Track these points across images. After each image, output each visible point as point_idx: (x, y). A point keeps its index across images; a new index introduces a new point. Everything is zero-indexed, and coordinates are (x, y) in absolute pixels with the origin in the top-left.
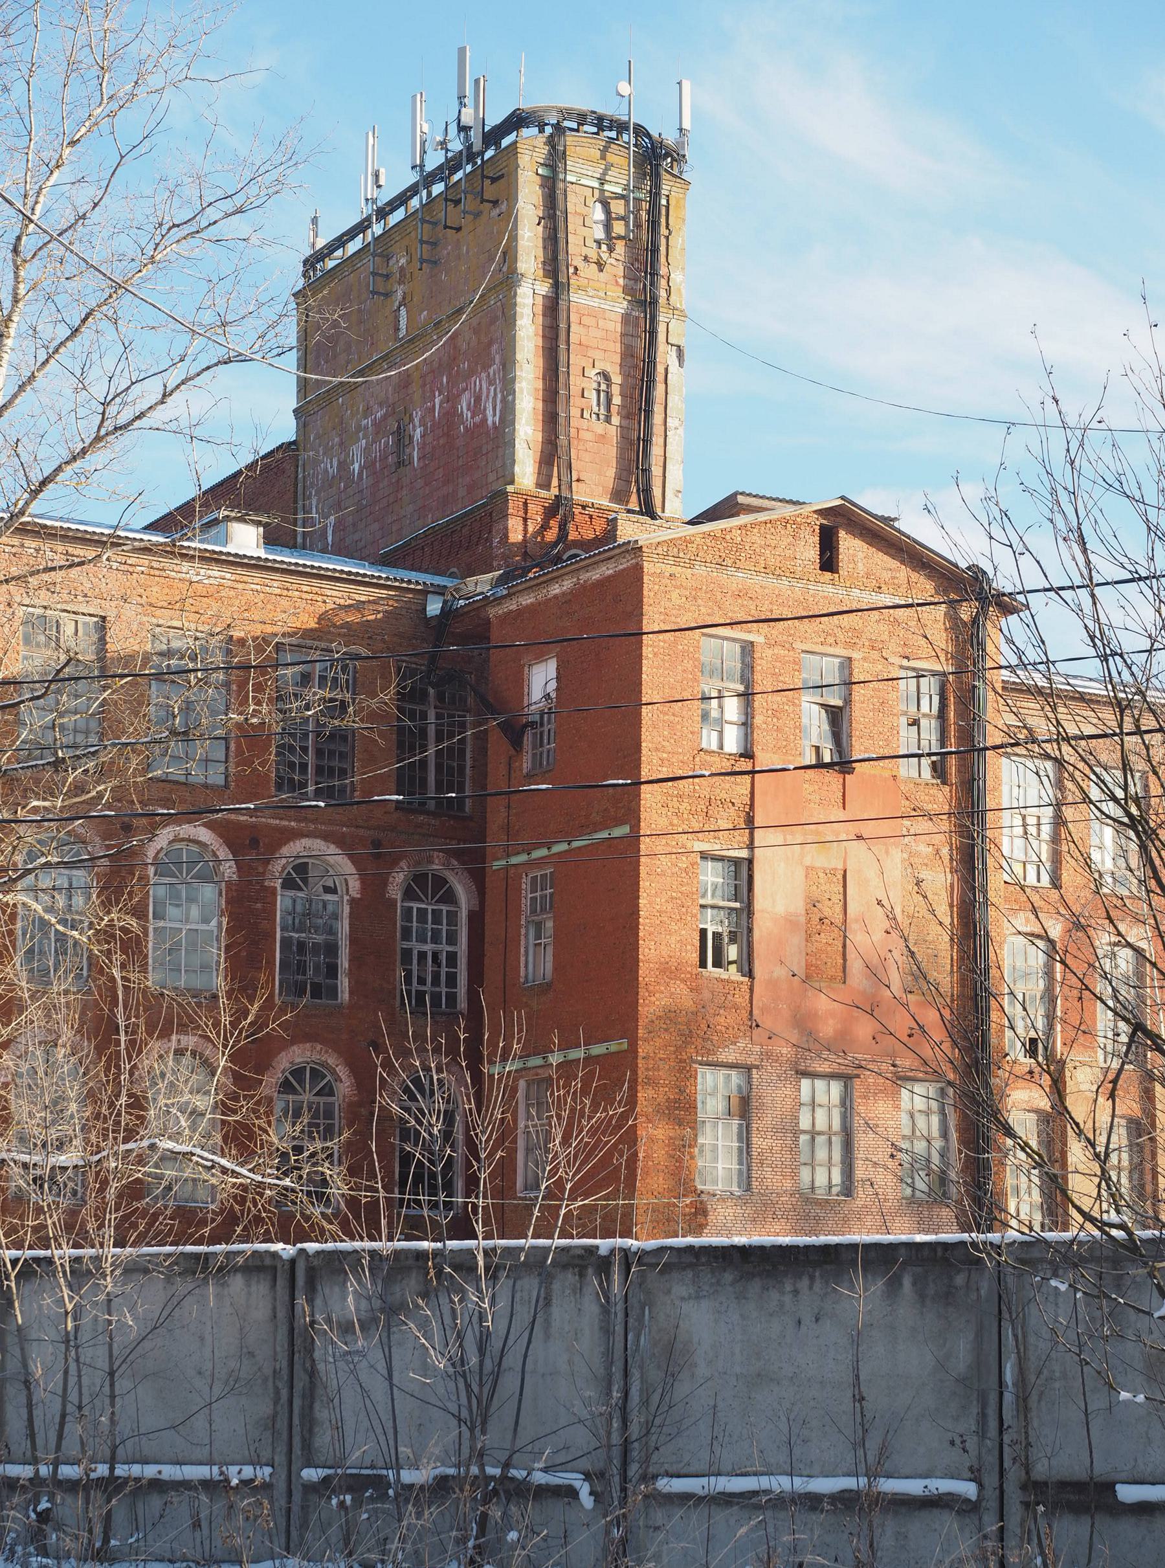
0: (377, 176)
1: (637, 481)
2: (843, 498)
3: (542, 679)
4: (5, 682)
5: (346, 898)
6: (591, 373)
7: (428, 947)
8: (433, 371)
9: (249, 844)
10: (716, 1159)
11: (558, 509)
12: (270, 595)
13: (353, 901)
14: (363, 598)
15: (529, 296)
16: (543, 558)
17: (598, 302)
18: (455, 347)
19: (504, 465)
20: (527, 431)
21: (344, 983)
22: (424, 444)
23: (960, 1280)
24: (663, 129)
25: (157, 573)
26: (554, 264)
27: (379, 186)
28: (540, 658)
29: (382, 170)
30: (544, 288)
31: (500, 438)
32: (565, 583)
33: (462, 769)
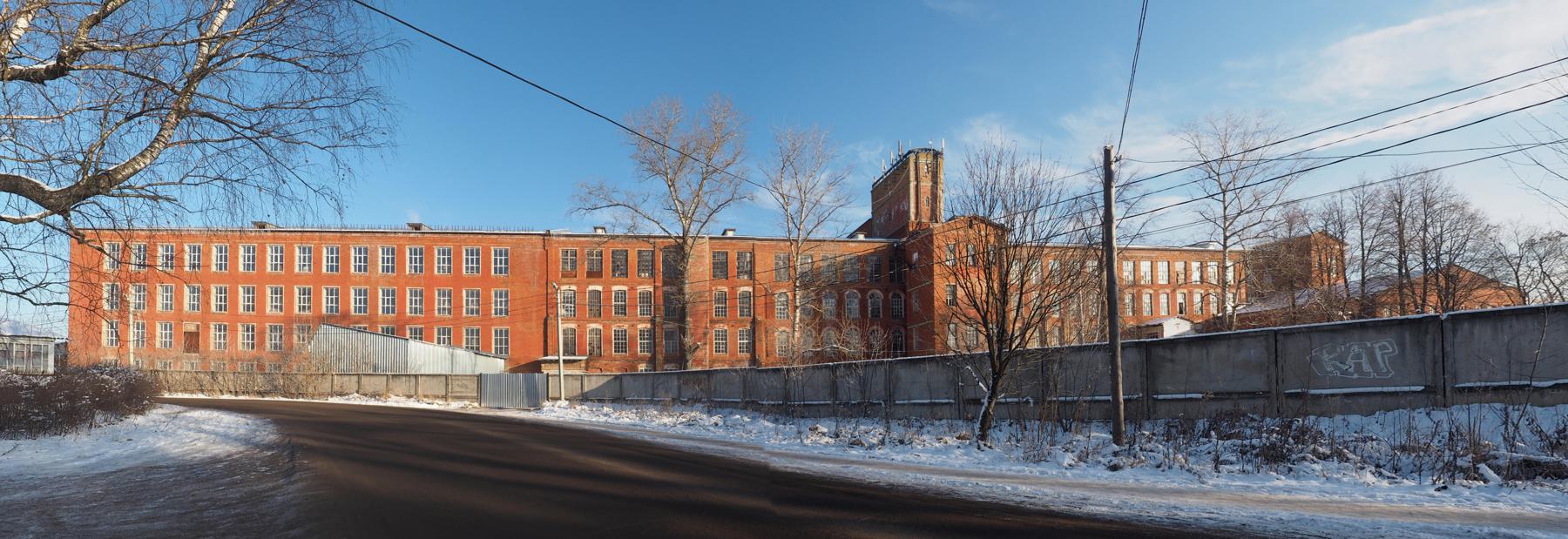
1: (934, 217)
3: (915, 256)
4: (1557, 473)
9: (863, 292)
10: (951, 342)
11: (919, 224)
12: (865, 246)
15: (912, 185)
16: (915, 233)
17: (926, 184)
20: (913, 210)
23: (300, 378)
24: (938, 149)
31: (908, 212)
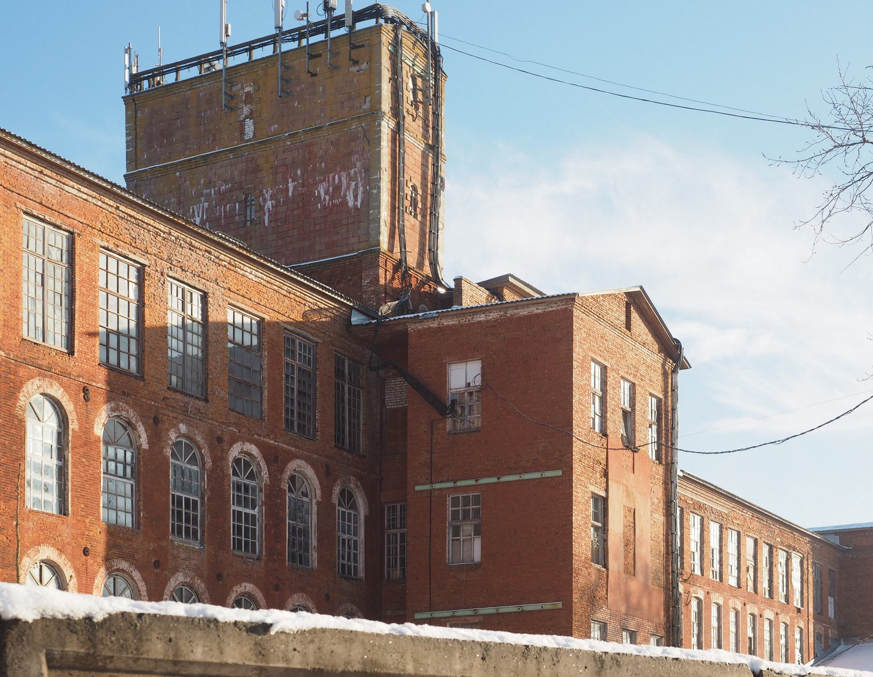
0: (227, 28)
2: (641, 287)
5: (314, 501)
6: (410, 184)
7: (346, 536)
8: (286, 166)
13: (318, 503)
14: (322, 306)
18: (310, 152)
19: (368, 234)
21: (314, 555)
22: (276, 213)
25: (232, 268)
26: (397, 112)
27: (227, 36)
28: (464, 357)
29: (230, 25)
30: (392, 124)
32: (492, 314)
33: (359, 424)
